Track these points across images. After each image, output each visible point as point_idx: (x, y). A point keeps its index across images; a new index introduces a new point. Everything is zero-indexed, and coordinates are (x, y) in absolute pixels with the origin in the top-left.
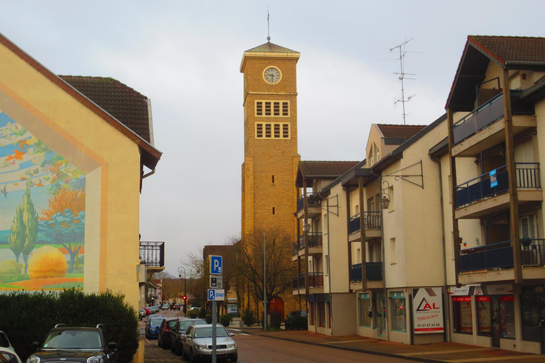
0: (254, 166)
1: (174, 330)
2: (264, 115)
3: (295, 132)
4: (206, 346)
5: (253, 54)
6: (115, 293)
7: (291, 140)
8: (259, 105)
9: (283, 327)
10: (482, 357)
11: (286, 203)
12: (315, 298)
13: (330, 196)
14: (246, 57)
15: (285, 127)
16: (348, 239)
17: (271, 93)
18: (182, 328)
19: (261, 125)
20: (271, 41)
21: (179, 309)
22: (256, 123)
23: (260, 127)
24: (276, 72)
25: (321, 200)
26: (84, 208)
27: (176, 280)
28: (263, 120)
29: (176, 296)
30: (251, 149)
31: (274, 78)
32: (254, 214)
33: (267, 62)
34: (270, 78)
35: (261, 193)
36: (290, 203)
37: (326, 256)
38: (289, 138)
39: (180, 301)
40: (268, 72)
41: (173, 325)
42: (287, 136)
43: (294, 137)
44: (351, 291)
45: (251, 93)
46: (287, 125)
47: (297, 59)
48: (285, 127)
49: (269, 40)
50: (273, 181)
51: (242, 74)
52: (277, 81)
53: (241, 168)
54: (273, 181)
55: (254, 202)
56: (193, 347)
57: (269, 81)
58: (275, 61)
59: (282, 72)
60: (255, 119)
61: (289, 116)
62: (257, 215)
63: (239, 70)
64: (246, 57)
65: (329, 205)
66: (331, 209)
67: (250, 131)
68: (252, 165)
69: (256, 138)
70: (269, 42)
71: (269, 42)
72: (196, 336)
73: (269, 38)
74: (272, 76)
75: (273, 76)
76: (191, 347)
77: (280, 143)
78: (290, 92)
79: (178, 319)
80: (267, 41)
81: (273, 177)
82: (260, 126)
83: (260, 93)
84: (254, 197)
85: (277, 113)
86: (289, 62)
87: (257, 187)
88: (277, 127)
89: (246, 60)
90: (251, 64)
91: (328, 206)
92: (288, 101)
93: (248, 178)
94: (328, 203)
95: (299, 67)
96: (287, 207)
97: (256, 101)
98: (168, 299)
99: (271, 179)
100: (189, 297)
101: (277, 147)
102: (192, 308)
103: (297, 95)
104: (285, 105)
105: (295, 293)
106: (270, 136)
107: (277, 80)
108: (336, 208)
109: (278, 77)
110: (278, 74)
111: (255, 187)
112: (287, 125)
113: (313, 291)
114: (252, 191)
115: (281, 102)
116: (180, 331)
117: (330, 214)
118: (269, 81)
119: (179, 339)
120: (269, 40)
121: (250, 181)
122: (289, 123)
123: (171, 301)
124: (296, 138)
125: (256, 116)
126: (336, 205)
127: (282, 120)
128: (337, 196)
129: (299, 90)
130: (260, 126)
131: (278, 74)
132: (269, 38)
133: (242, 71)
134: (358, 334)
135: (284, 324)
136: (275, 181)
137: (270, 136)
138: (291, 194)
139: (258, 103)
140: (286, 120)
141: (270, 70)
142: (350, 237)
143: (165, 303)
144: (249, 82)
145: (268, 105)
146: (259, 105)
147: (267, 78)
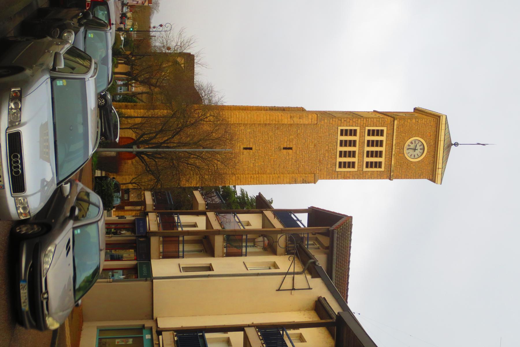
0: (304, 125)
1: (86, 15)
2: (367, 138)
3: (345, 177)
4: (20, 125)
5: (443, 127)
7: (335, 171)
8: (380, 133)
9: (98, 173)
10: (70, 335)
11: (257, 165)
12: (142, 237)
13: (309, 277)
14: (439, 117)
15: (352, 165)
16: (249, 326)
17: (394, 147)
18: (90, 35)
19: (355, 135)
21: (121, 23)
22: (358, 129)
23: (353, 133)
25: (304, 263)
27: (148, 22)
28: (362, 136)
29: (134, 20)
30: (326, 121)
31: (411, 151)
32: (244, 124)
33: (432, 143)
34: (412, 146)
35: (271, 134)
36: (257, 170)
37: (210, 268)
38: (338, 169)
39: (129, 23)
40: (420, 144)
41: (101, 15)
42: (340, 167)
43: (339, 176)
44: (159, 332)
45: (396, 122)
46: (353, 167)
47: (433, 180)
48: (352, 165)
49: (455, 144)
50: (284, 148)
52: (408, 155)
53: (299, 106)
54: (284, 148)
55: (259, 124)
56: (19, 76)
57: (409, 145)
58: (433, 153)
59: (419, 162)
60: (362, 127)
61: (365, 169)
62: (243, 128)
63: (417, 106)
64: (439, 117)
65: (295, 276)
66: (289, 278)
67: (348, 120)
68: (307, 122)
69: (340, 128)
70: (452, 145)
72: (60, 83)
73: (456, 144)
74: (415, 150)
75: (414, 151)
76: (21, 70)
77: (331, 158)
78: (393, 171)
79: (110, 24)
80: (453, 143)
81: (290, 148)
82: (354, 133)
83: (395, 134)
84: (266, 124)
85: (370, 154)
86: (431, 171)
87: (278, 128)
88: (352, 154)
89: (437, 117)
90: (428, 125)
91: (294, 273)
92: (382, 169)
93: (291, 117)
94: (298, 273)
95: (425, 182)
96: (252, 165)
97: (385, 129)
98: (131, 11)
99: (288, 146)
100: (134, 35)
101: (327, 155)
102: (122, 39)
103: (390, 179)
104: (378, 165)
105: (148, 197)
106: (341, 145)
107: (409, 155)
108: (291, 288)
109: (413, 157)
110: (416, 156)
111: (279, 126)
112: (353, 167)
113: (155, 243)
114: (274, 122)
115: (382, 160)
116: (82, 29)
117: (281, 277)
118: (409, 145)
119: (64, 28)
120: (455, 144)
121: (286, 119)
122: (356, 169)
123: (129, 15)
124: (337, 178)
125: (367, 128)
126: (296, 287)
127: (361, 161)
128: (310, 289)
130: (354, 133)
131: (416, 156)
132: (456, 144)
133: (415, 109)
134: (85, 325)
135: (104, 175)
136: (285, 151)
137: (341, 145)
138: (268, 171)
139: (382, 131)
141: (422, 147)
142: (253, 329)
143: (128, 8)
144: (409, 120)
145: (379, 143)
146: (380, 133)
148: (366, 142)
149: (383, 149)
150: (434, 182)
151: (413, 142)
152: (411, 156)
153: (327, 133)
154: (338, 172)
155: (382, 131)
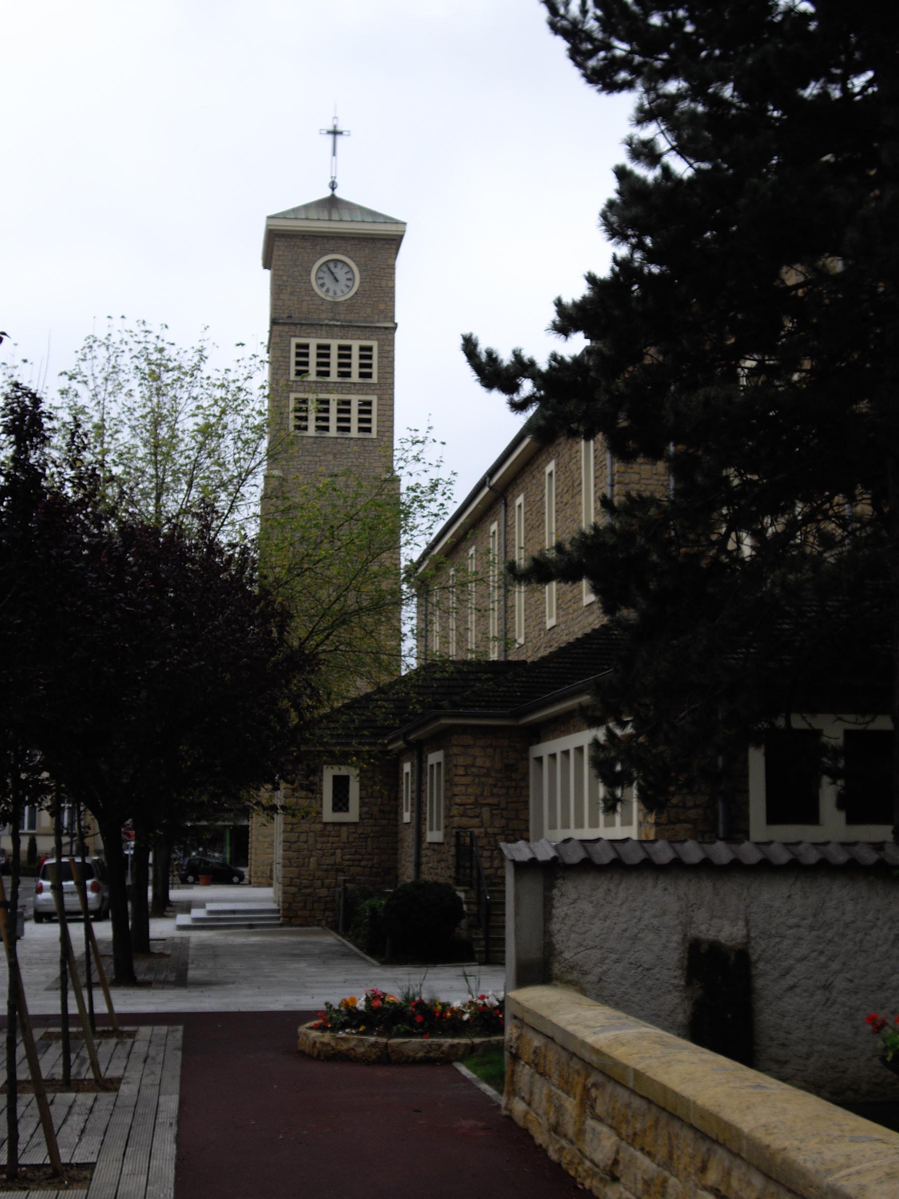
6: (567, 53)
20: (339, 193)
24: (346, 269)
26: (527, 830)
49: (333, 189)
51: (268, 273)
53: (464, 358)
63: (260, 262)
70: (333, 196)
71: (333, 196)
73: (333, 186)
80: (327, 193)
90: (290, 245)
92: (374, 344)
97: (294, 341)
103: (395, 328)
109: (349, 283)
110: (349, 276)
120: (333, 189)
122: (374, 399)
129: (400, 316)
132: (333, 186)
140: (370, 388)
147: (322, 285)
148: (320, 379)
149: (356, 345)
150: (401, 237)
151: (321, 282)
152: (348, 287)
153: (823, 959)
154: (288, 397)
155: (299, 346)
